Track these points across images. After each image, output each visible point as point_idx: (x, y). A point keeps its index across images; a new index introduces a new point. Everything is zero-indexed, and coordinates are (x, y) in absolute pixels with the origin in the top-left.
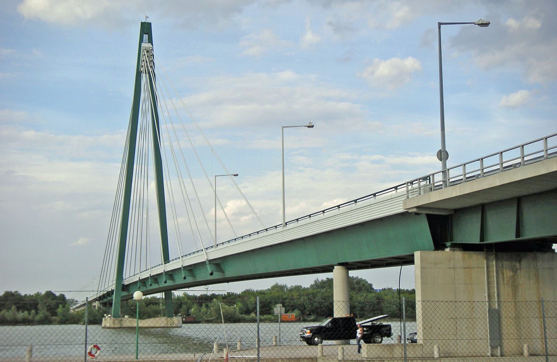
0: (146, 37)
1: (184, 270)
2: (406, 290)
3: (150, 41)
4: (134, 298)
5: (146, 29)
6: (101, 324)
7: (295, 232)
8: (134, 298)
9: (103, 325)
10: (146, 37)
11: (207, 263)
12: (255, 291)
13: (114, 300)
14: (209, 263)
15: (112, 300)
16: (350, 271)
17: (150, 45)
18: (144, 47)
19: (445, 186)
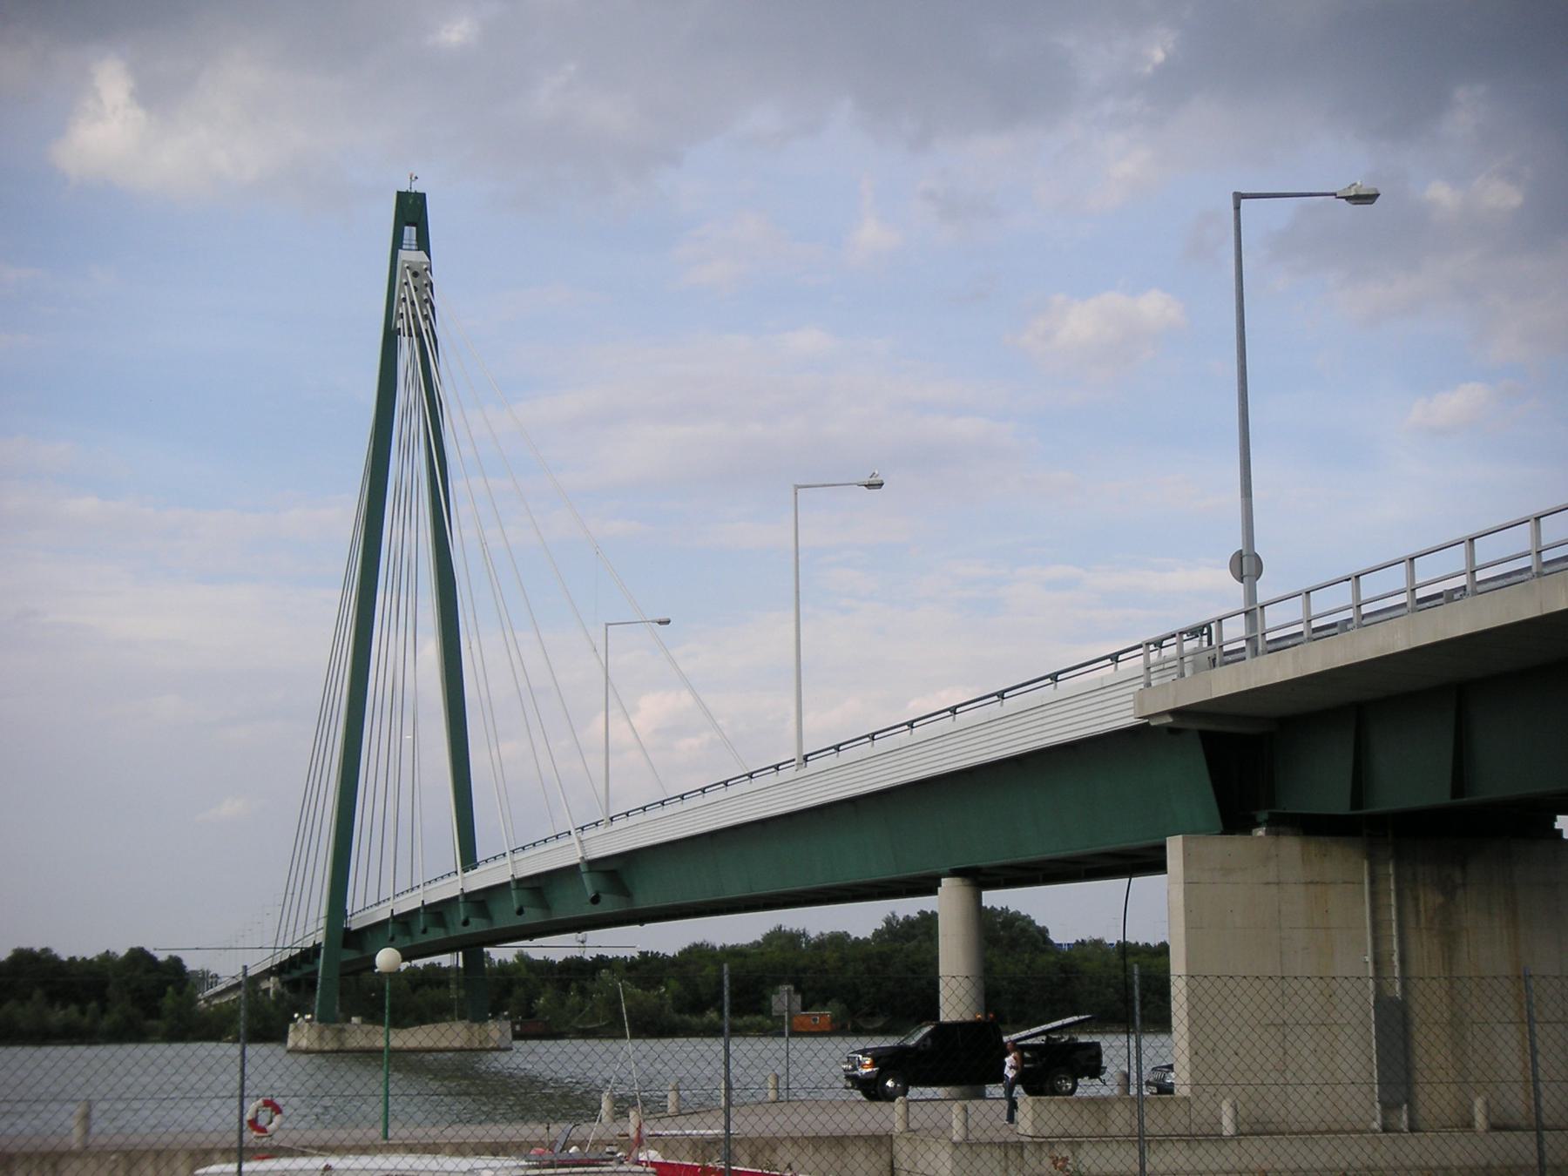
0: (410, 233)
3: (423, 243)
6: (286, 1042)
9: (290, 1044)
10: (410, 233)
15: (316, 972)
17: (422, 255)
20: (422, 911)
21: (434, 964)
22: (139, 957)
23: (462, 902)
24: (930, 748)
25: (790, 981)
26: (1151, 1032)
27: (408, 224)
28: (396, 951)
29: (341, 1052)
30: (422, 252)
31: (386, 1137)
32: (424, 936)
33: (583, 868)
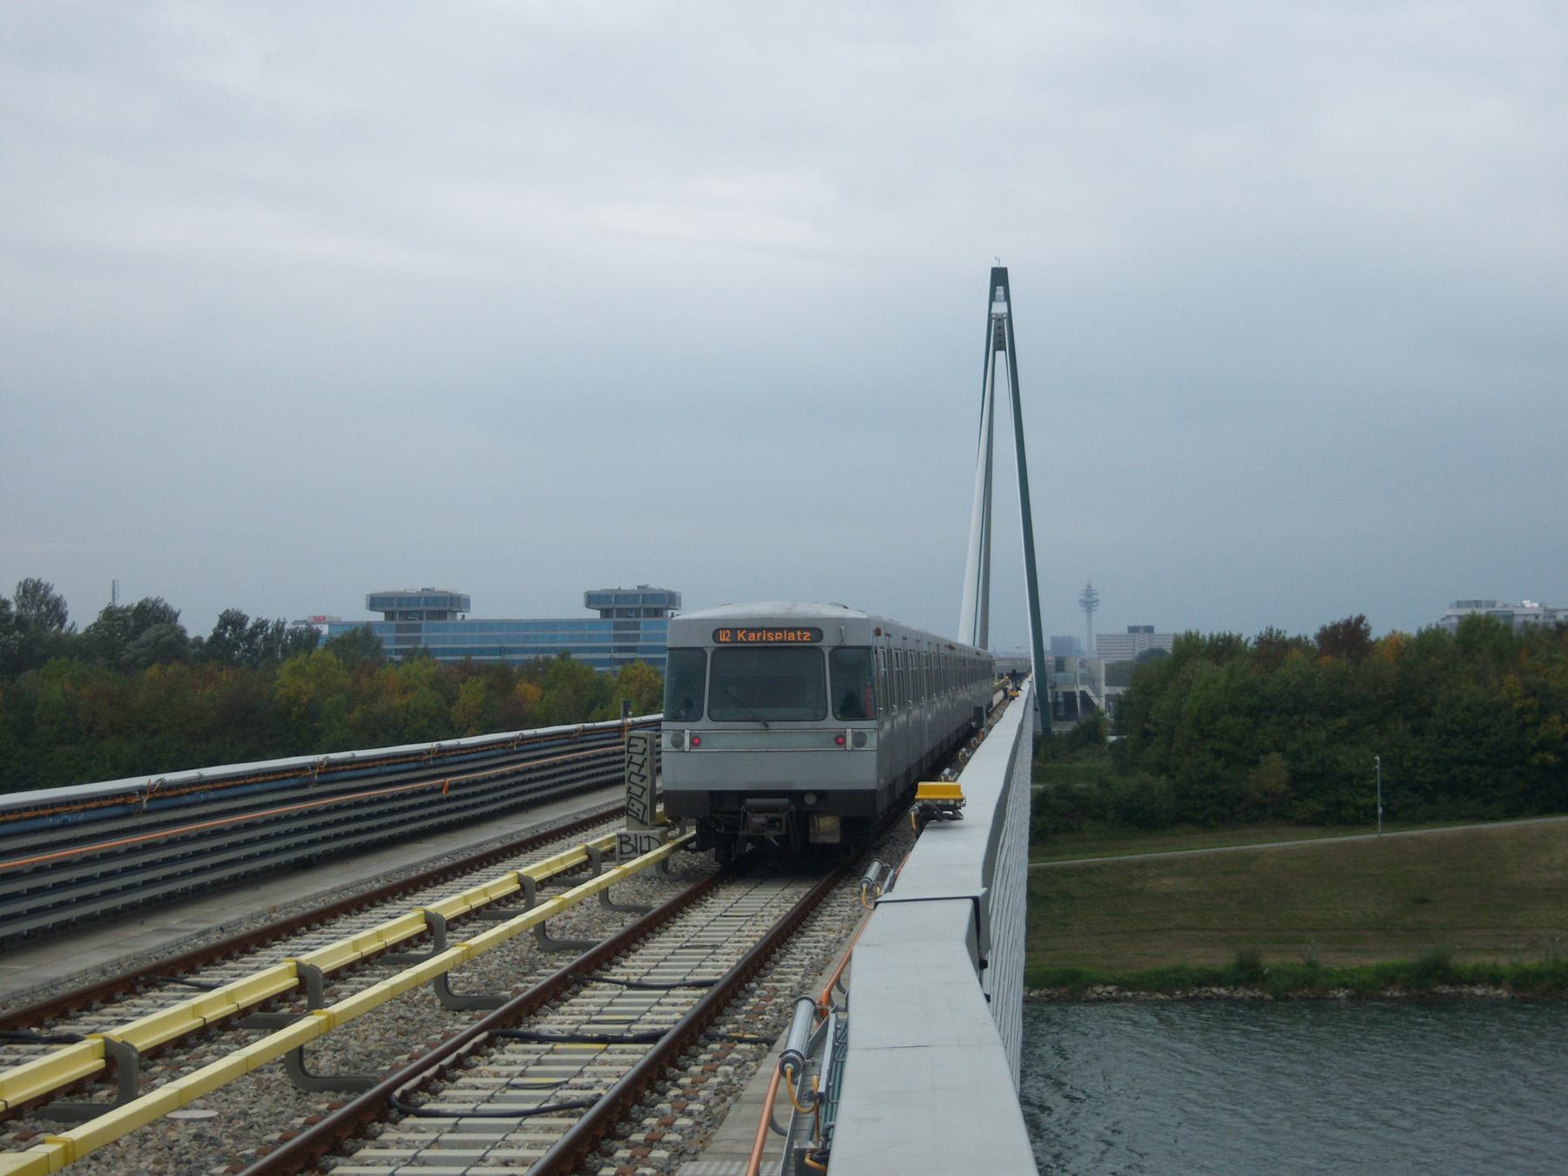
0: (1000, 291)
3: (1007, 298)
5: (999, 277)
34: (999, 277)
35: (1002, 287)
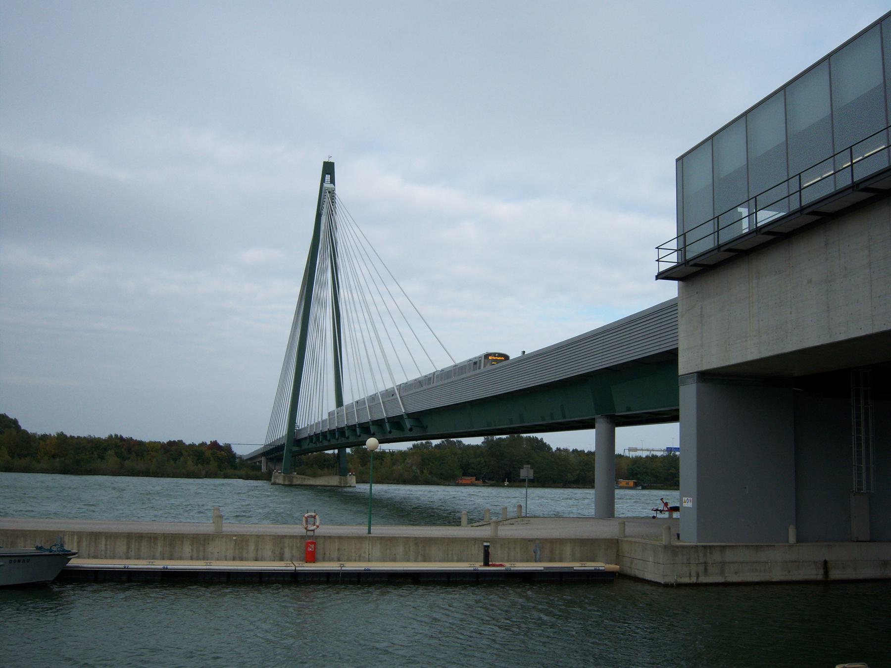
0: (328, 177)
1: (373, 425)
2: (556, 451)
3: (332, 181)
4: (365, 445)
5: (329, 169)
6: (271, 480)
7: (659, 333)
8: (365, 445)
9: (272, 481)
10: (328, 177)
11: (405, 417)
12: (114, 436)
13: (284, 455)
14: (408, 417)
15: (283, 454)
16: (618, 430)
17: (332, 186)
18: (326, 187)
19: (381, 439)
20: (328, 432)
21: (537, 438)
22: (215, 444)
23: (347, 430)
24: (591, 367)
25: (528, 463)
26: (586, 488)
27: (327, 174)
28: (377, 441)
29: (290, 485)
30: (332, 184)
31: (369, 533)
32: (389, 434)
33: (405, 417)
34: (329, 169)
35: (329, 176)
